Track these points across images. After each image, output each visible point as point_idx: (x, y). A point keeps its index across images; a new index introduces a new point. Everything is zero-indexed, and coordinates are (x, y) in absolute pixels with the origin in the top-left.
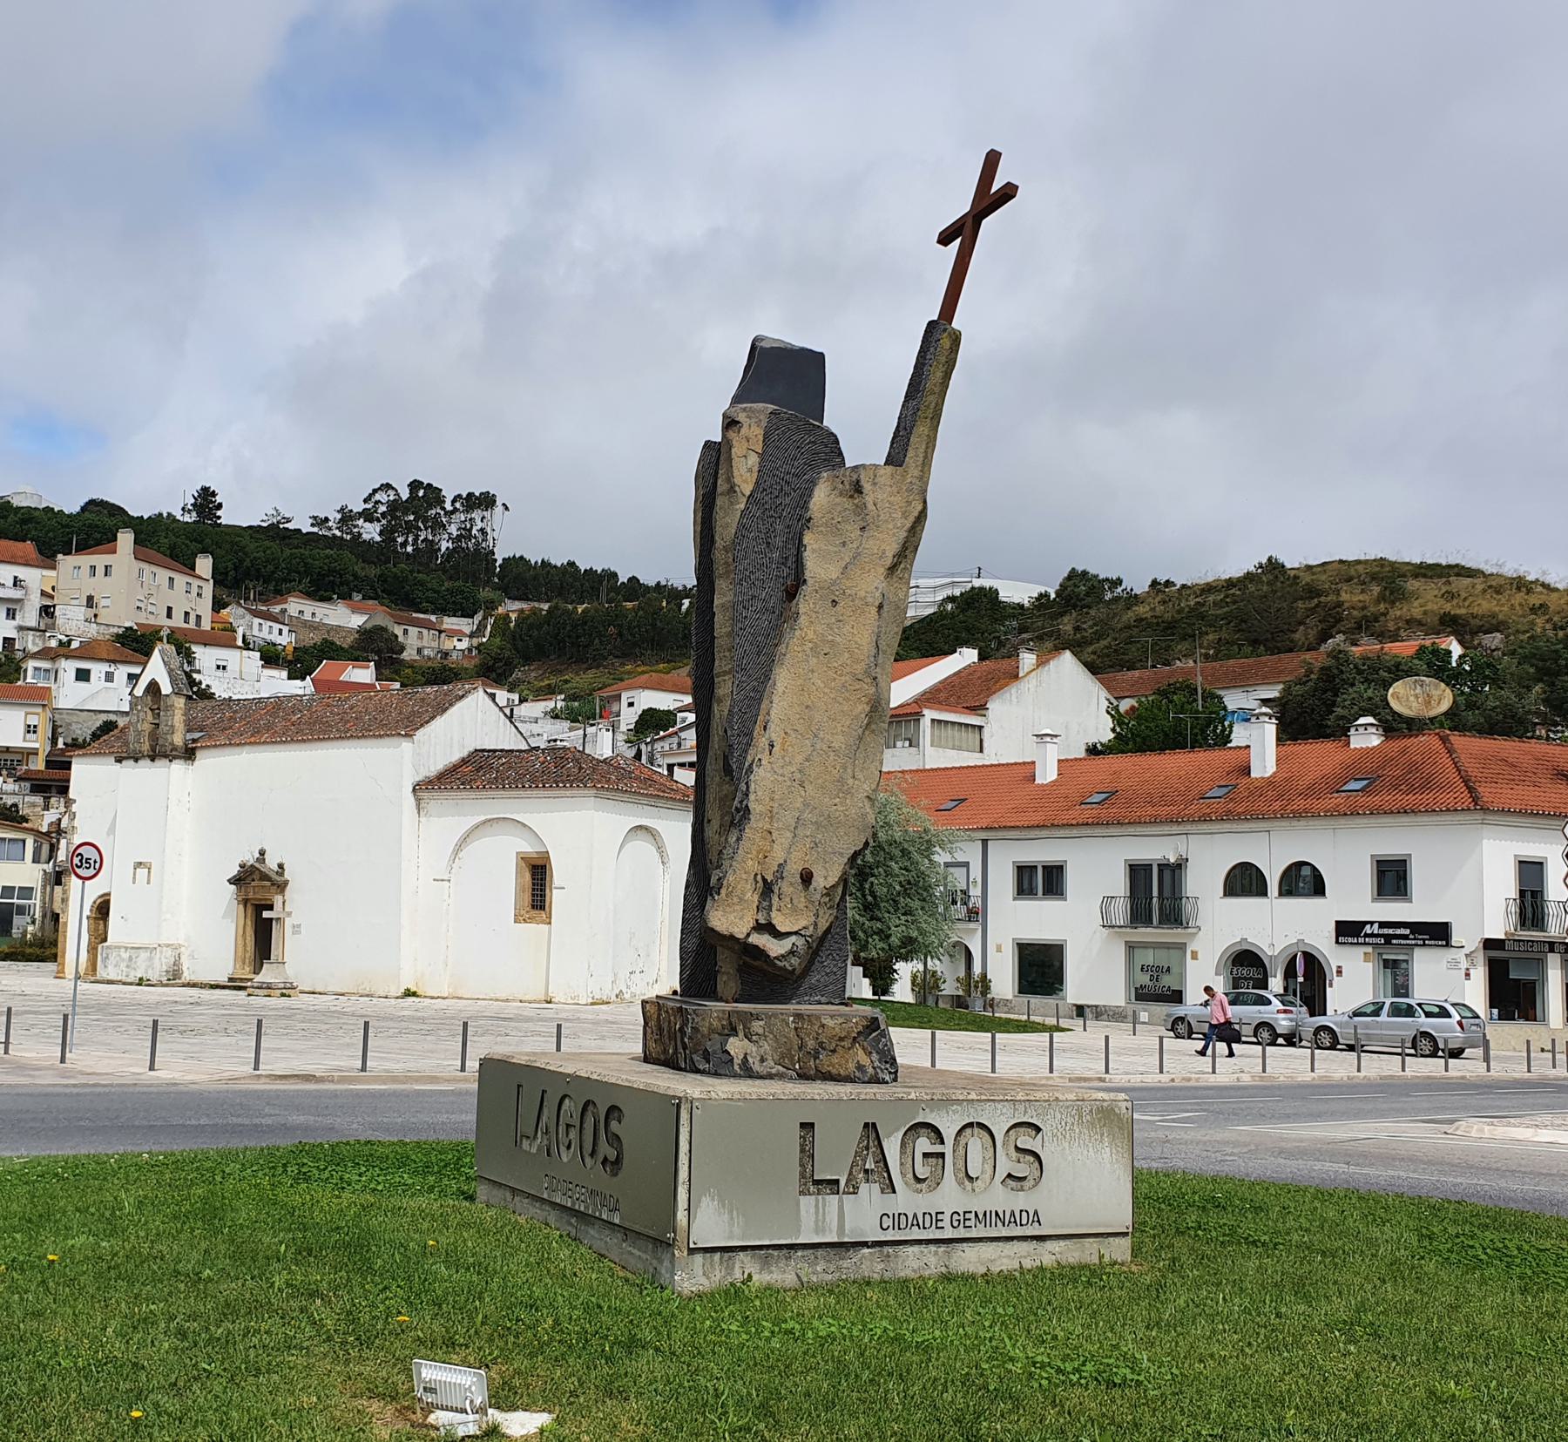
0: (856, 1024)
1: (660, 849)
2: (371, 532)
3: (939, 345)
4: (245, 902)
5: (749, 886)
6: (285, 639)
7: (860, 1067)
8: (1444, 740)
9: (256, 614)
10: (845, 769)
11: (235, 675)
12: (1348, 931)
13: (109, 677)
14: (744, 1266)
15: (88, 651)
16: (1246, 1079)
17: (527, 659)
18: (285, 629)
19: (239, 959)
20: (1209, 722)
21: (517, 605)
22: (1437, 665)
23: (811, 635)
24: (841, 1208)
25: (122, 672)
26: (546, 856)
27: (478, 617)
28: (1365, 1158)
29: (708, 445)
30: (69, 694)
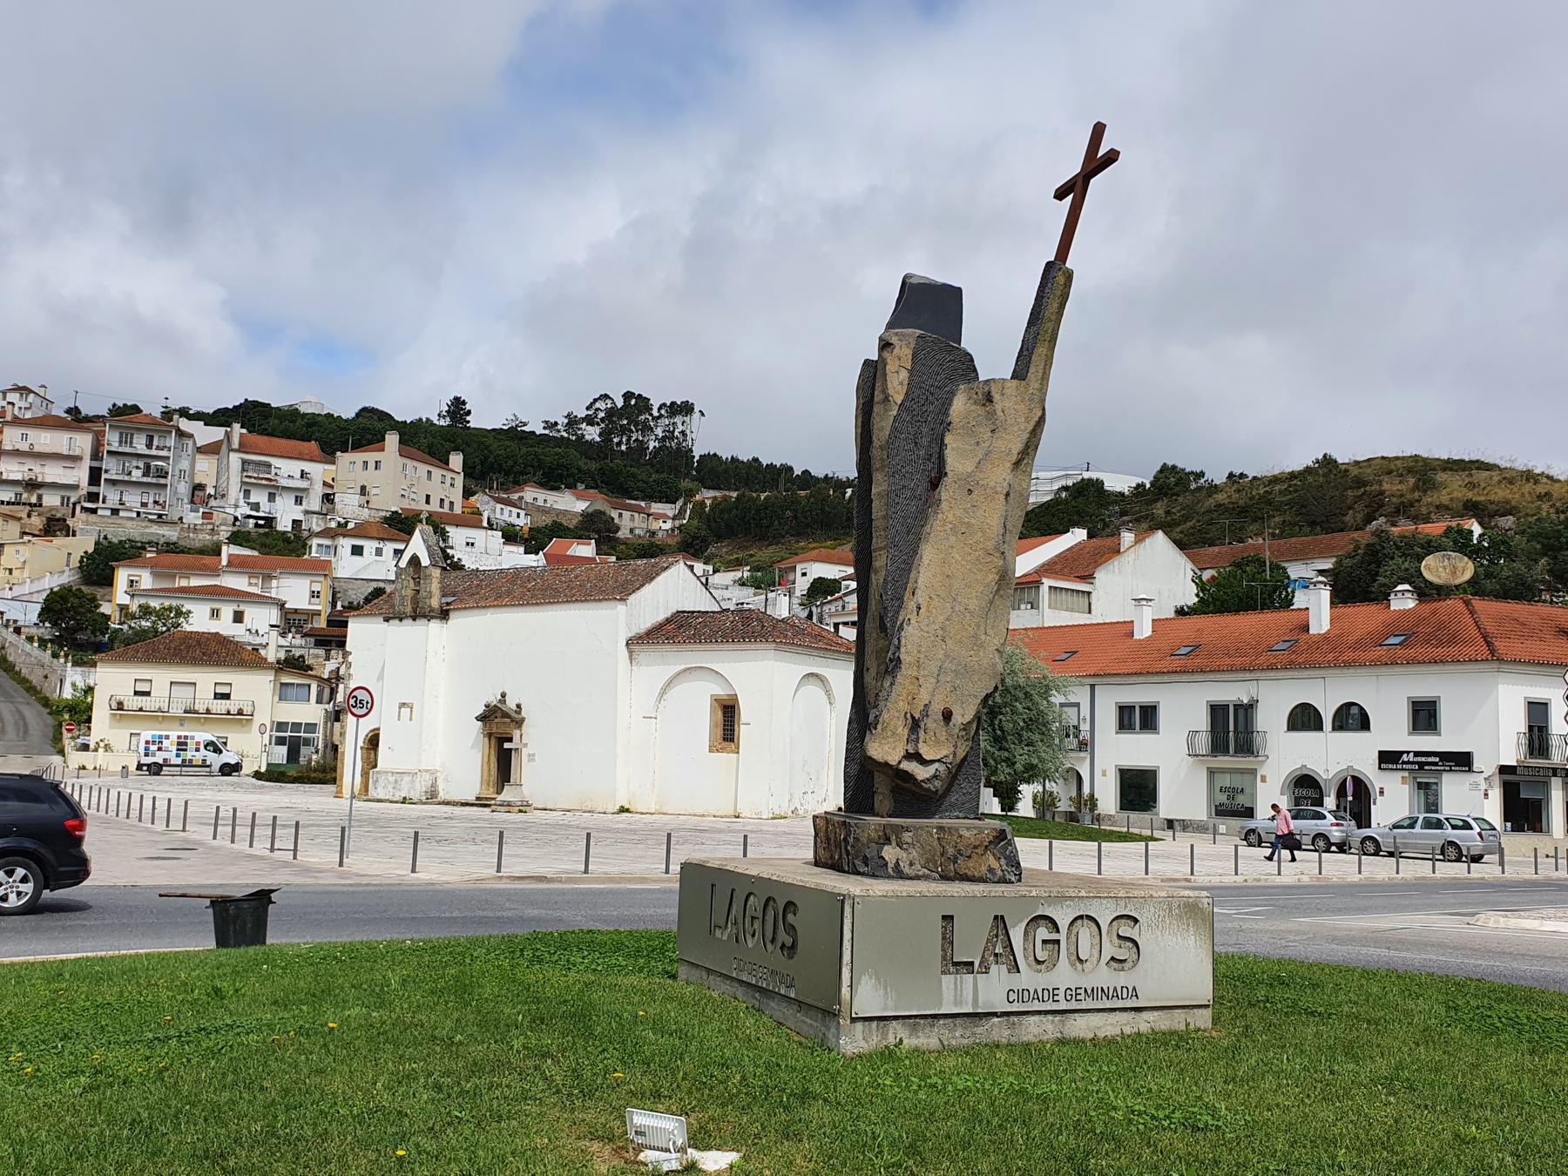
1: (828, 692)
2: (592, 433)
3: (1055, 281)
4: (490, 735)
6: (522, 521)
7: (991, 870)
8: (1467, 603)
9: (499, 500)
11: (482, 550)
12: (1388, 759)
13: (379, 552)
14: (897, 1032)
15: (362, 531)
16: (1305, 879)
17: (719, 538)
18: (522, 513)
19: (485, 782)
20: (1276, 589)
22: (1461, 541)
25: (389, 548)
26: (735, 698)
27: (680, 503)
28: (1403, 944)
29: (867, 363)
30: (346, 566)
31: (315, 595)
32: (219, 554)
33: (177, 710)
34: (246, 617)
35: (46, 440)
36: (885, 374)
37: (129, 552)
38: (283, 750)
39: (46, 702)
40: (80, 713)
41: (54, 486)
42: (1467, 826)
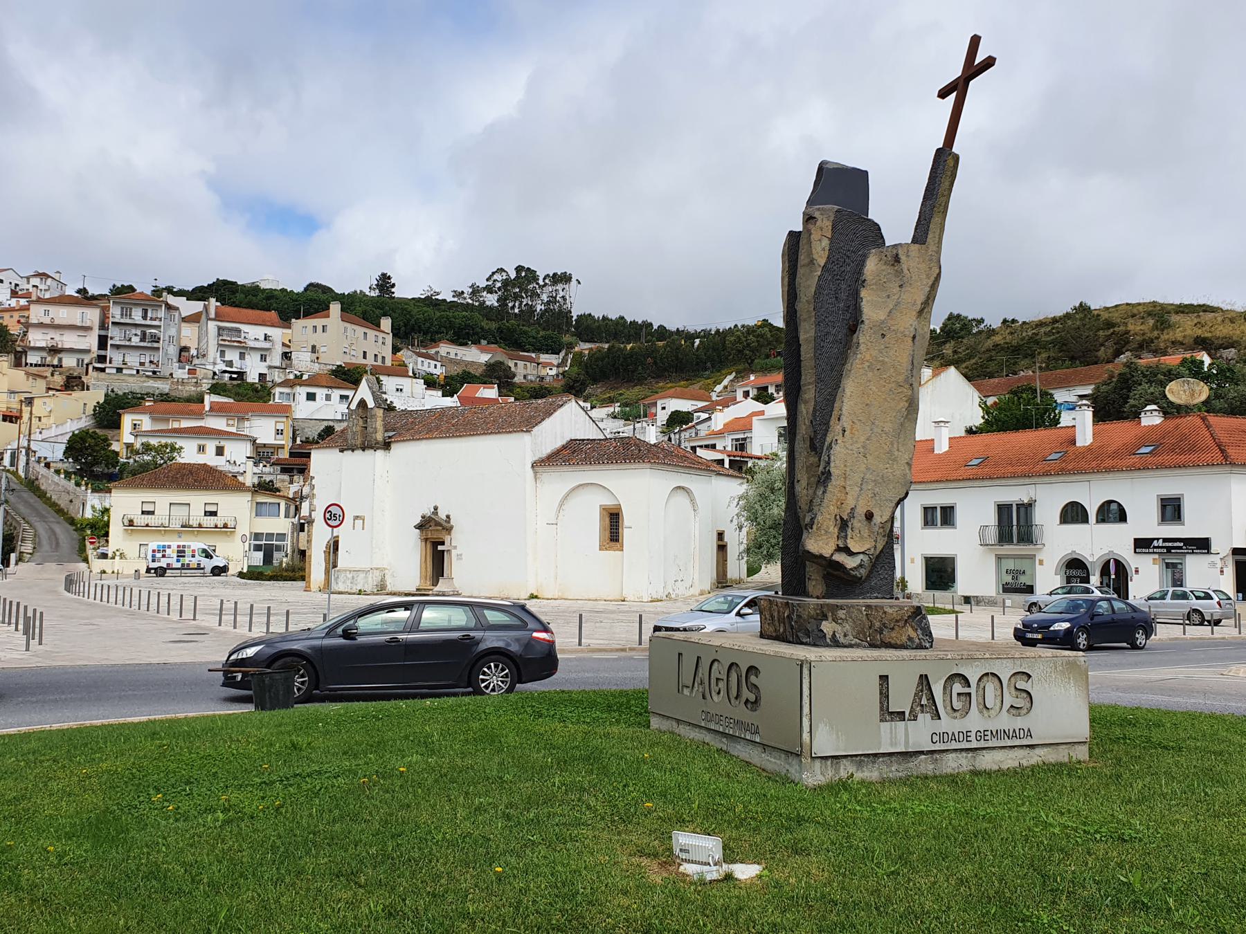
1: (693, 501)
2: (491, 300)
3: (945, 164)
4: (426, 540)
5: (832, 523)
6: (438, 371)
7: (910, 639)
8: (1204, 419)
10: (892, 444)
11: (410, 395)
12: (1142, 545)
13: (328, 398)
15: (314, 381)
17: (595, 381)
18: (439, 364)
19: (423, 577)
20: (1046, 410)
22: (1195, 370)
23: (868, 357)
24: (906, 729)
25: (335, 394)
26: (619, 507)
27: (562, 354)
29: (791, 234)
30: (303, 409)
31: (279, 432)
32: (202, 402)
33: (176, 525)
34: (226, 452)
35: (63, 314)
36: (809, 242)
37: (132, 401)
38: (260, 555)
39: (72, 521)
40: (100, 529)
41: (71, 351)
42: (1208, 597)
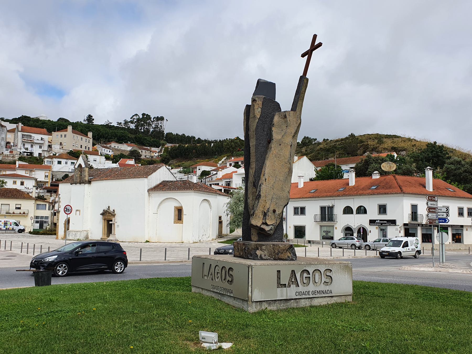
0: (287, 247)
1: (210, 205)
2: (132, 126)
3: (303, 82)
4: (105, 219)
5: (261, 214)
6: (111, 153)
7: (288, 257)
8: (394, 177)
9: (103, 147)
11: (99, 163)
12: (372, 222)
13: (66, 163)
14: (264, 306)
15: (61, 156)
16: (351, 257)
17: (173, 158)
18: (111, 151)
19: (104, 234)
20: (338, 173)
21: (170, 145)
22: (391, 159)
23: (275, 152)
25: (69, 162)
26: (182, 207)
27: (160, 148)
28: (382, 275)
29: (247, 106)
30: (56, 167)
31: (46, 176)
36: (254, 109)
38: (38, 225)
